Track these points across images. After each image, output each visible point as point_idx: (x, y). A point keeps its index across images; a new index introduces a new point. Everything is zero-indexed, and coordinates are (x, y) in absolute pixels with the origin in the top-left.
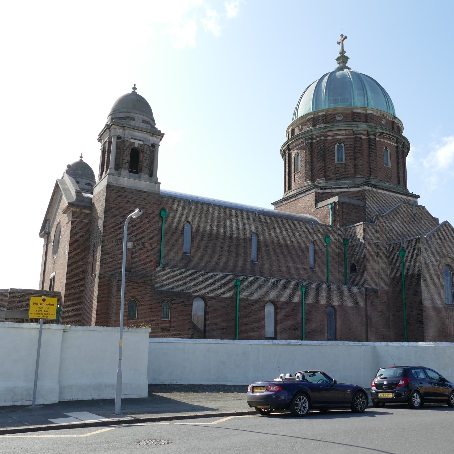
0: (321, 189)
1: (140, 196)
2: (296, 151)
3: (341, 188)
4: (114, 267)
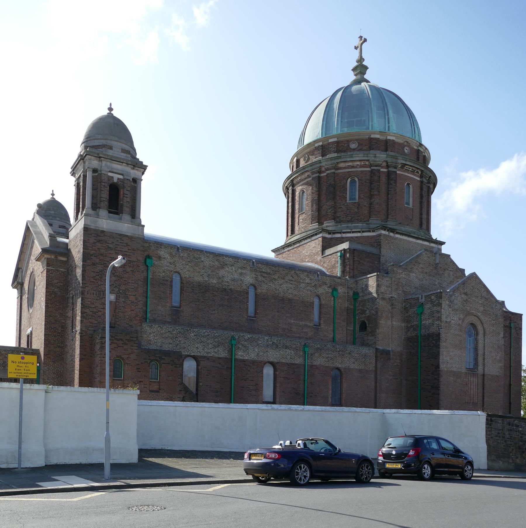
0: (330, 233)
1: (121, 241)
2: (301, 187)
3: (353, 232)
4: (96, 322)
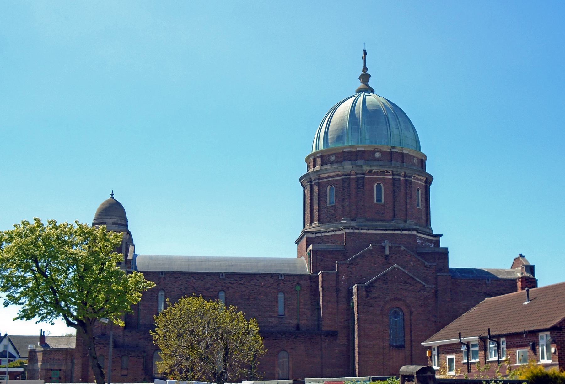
0: (313, 234)
